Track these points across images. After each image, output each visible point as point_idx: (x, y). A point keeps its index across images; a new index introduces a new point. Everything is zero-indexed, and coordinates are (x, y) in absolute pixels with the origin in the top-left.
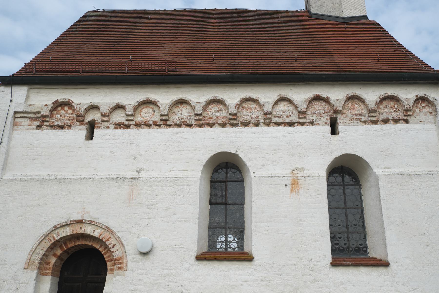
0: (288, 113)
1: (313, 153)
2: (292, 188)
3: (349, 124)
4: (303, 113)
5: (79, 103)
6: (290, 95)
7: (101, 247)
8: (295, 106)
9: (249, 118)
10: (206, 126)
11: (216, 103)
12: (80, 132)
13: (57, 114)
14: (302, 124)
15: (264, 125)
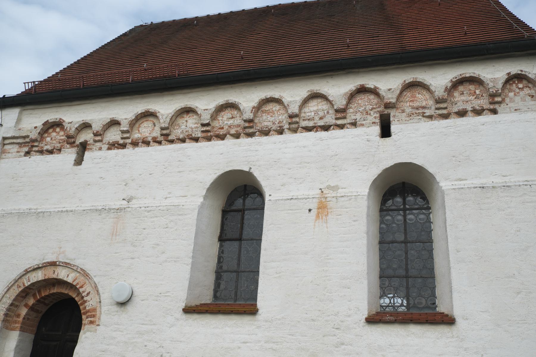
0: (321, 114)
1: (352, 164)
2: (318, 213)
3: (407, 122)
4: (341, 112)
5: (70, 121)
6: (326, 90)
7: (77, 296)
8: (330, 102)
9: (269, 124)
10: (215, 139)
11: (229, 109)
12: (69, 155)
13: (48, 137)
14: (342, 127)
15: (290, 132)
